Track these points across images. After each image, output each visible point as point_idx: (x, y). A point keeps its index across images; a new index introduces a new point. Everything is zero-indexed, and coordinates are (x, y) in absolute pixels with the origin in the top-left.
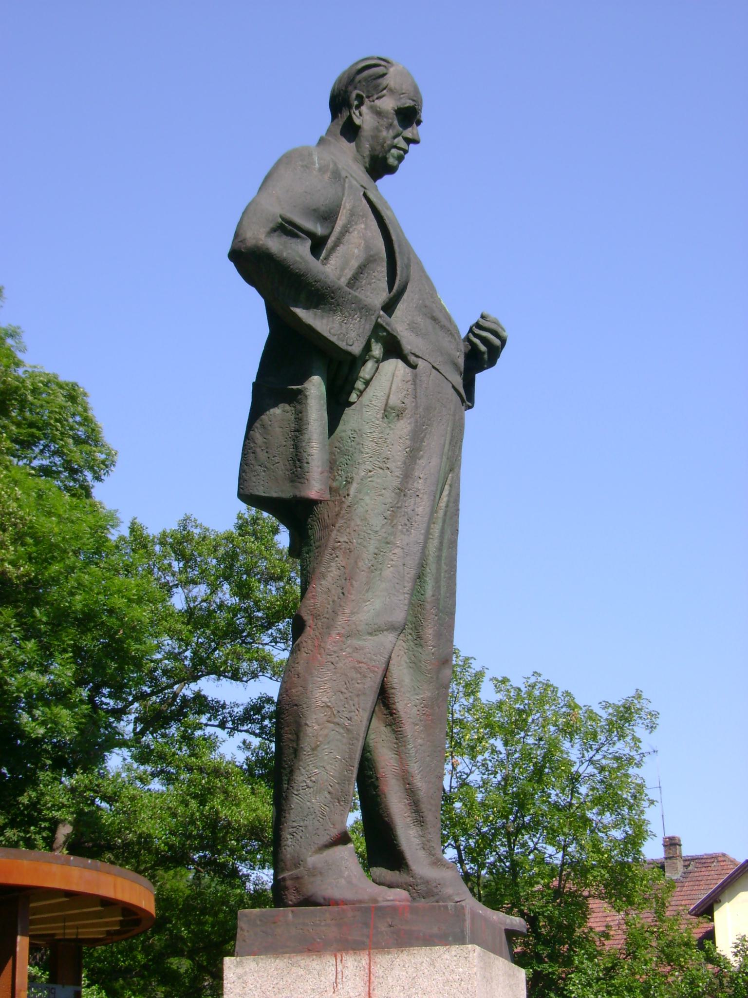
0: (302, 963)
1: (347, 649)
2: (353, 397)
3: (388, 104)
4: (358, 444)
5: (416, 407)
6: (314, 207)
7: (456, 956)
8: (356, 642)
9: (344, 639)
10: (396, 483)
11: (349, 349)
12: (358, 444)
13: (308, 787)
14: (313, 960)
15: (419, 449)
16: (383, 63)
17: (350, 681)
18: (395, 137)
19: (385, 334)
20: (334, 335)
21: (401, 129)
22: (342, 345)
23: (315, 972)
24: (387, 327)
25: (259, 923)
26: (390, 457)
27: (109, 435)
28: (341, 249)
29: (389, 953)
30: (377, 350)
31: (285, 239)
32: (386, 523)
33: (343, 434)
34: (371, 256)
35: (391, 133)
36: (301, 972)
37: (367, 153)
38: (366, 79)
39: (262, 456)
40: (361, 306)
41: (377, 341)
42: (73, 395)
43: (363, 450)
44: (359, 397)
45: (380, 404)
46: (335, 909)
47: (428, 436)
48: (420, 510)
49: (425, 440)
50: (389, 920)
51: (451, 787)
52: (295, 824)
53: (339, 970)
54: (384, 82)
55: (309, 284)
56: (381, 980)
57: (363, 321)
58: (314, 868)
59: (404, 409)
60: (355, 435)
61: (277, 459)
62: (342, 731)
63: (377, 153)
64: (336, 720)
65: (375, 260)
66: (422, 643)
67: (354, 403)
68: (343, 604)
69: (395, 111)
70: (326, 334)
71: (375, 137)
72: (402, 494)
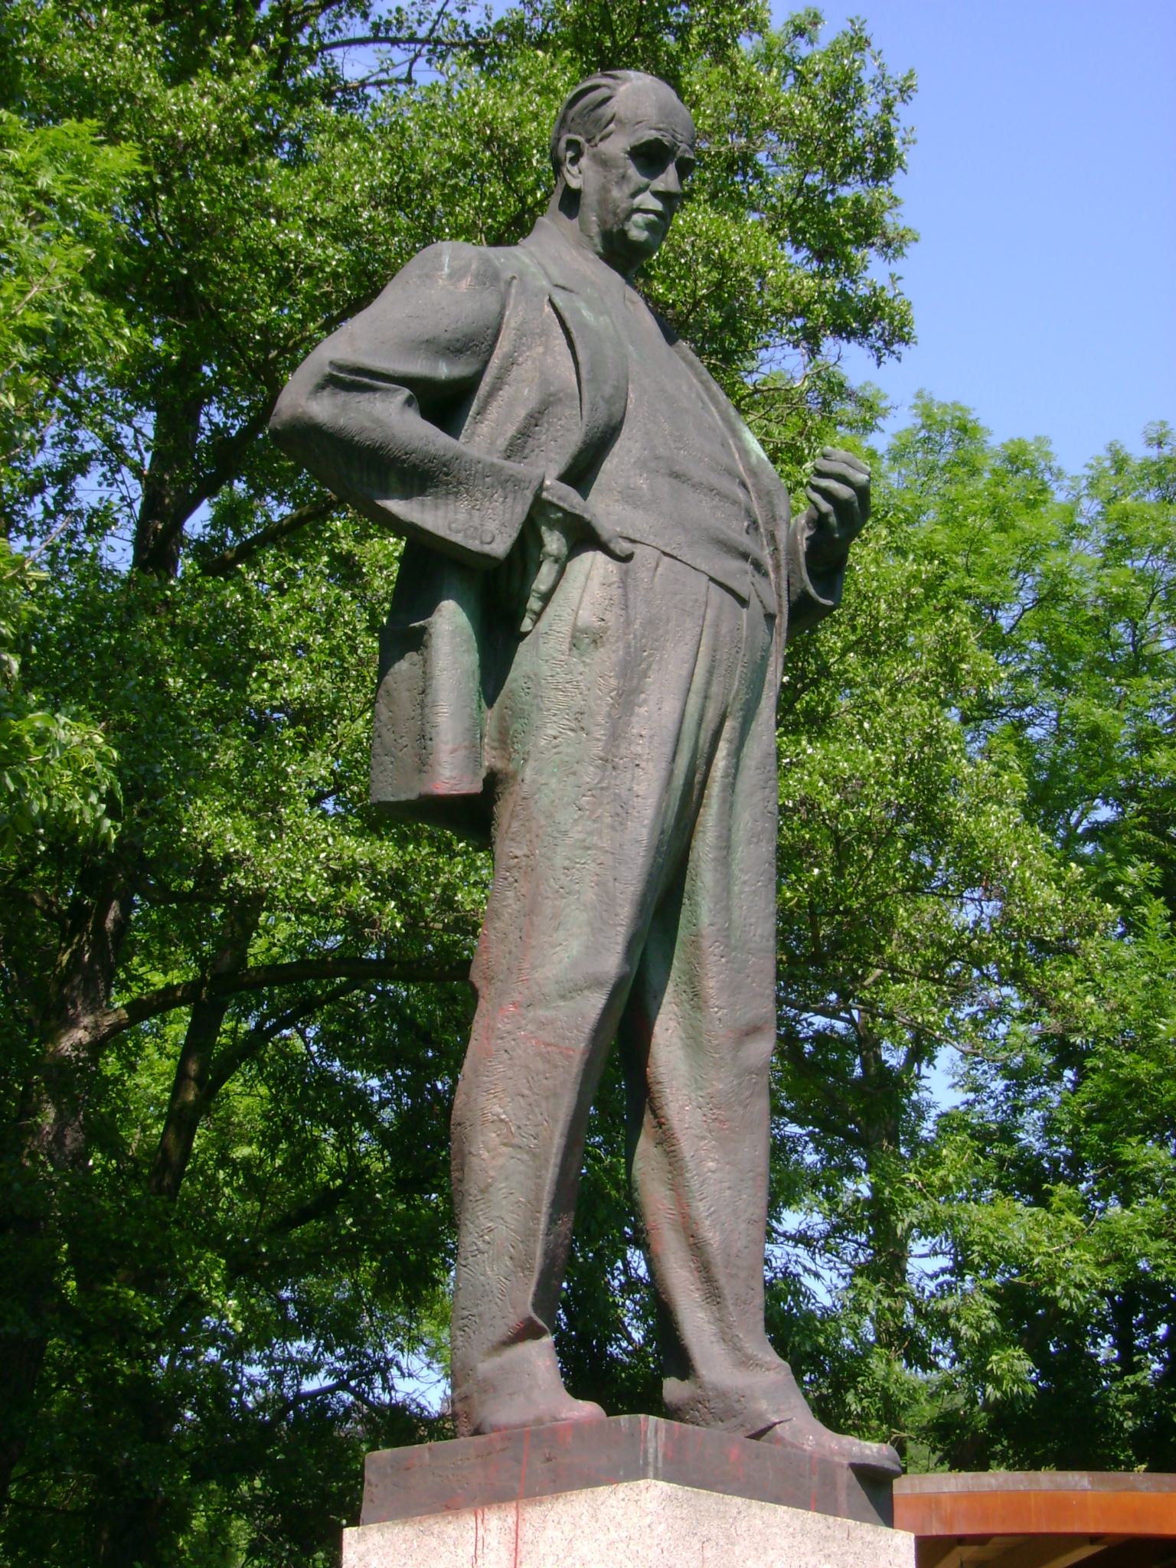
0: (436, 1529)
1: (529, 1027)
2: (526, 624)
3: (617, 145)
4: (536, 697)
5: (628, 623)
6: (426, 337)
8: (542, 1013)
9: (524, 1011)
10: (597, 750)
11: (487, 549)
12: (536, 697)
13: (482, 1252)
15: (638, 690)
18: (634, 195)
19: (560, 515)
20: (458, 532)
21: (646, 180)
22: (474, 545)
23: (450, 1542)
24: (561, 504)
25: (389, 1471)
26: (586, 710)
28: (505, 393)
30: (554, 542)
31: (343, 396)
32: (581, 817)
33: (514, 685)
34: (551, 395)
35: (627, 190)
36: (434, 1542)
37: (595, 230)
38: (581, 114)
39: (388, 737)
41: (551, 528)
44: (535, 622)
45: (566, 629)
47: (655, 667)
48: (640, 788)
49: (650, 673)
50: (547, 1451)
51: (934, 1253)
52: (466, 1313)
54: (607, 110)
55: (396, 460)
57: (509, 500)
59: (605, 630)
60: (530, 684)
61: (404, 741)
62: (525, 1157)
63: (608, 226)
64: (516, 1141)
65: (560, 400)
66: (701, 1004)
67: (527, 634)
69: (629, 153)
70: (442, 531)
71: (603, 202)
72: (609, 766)
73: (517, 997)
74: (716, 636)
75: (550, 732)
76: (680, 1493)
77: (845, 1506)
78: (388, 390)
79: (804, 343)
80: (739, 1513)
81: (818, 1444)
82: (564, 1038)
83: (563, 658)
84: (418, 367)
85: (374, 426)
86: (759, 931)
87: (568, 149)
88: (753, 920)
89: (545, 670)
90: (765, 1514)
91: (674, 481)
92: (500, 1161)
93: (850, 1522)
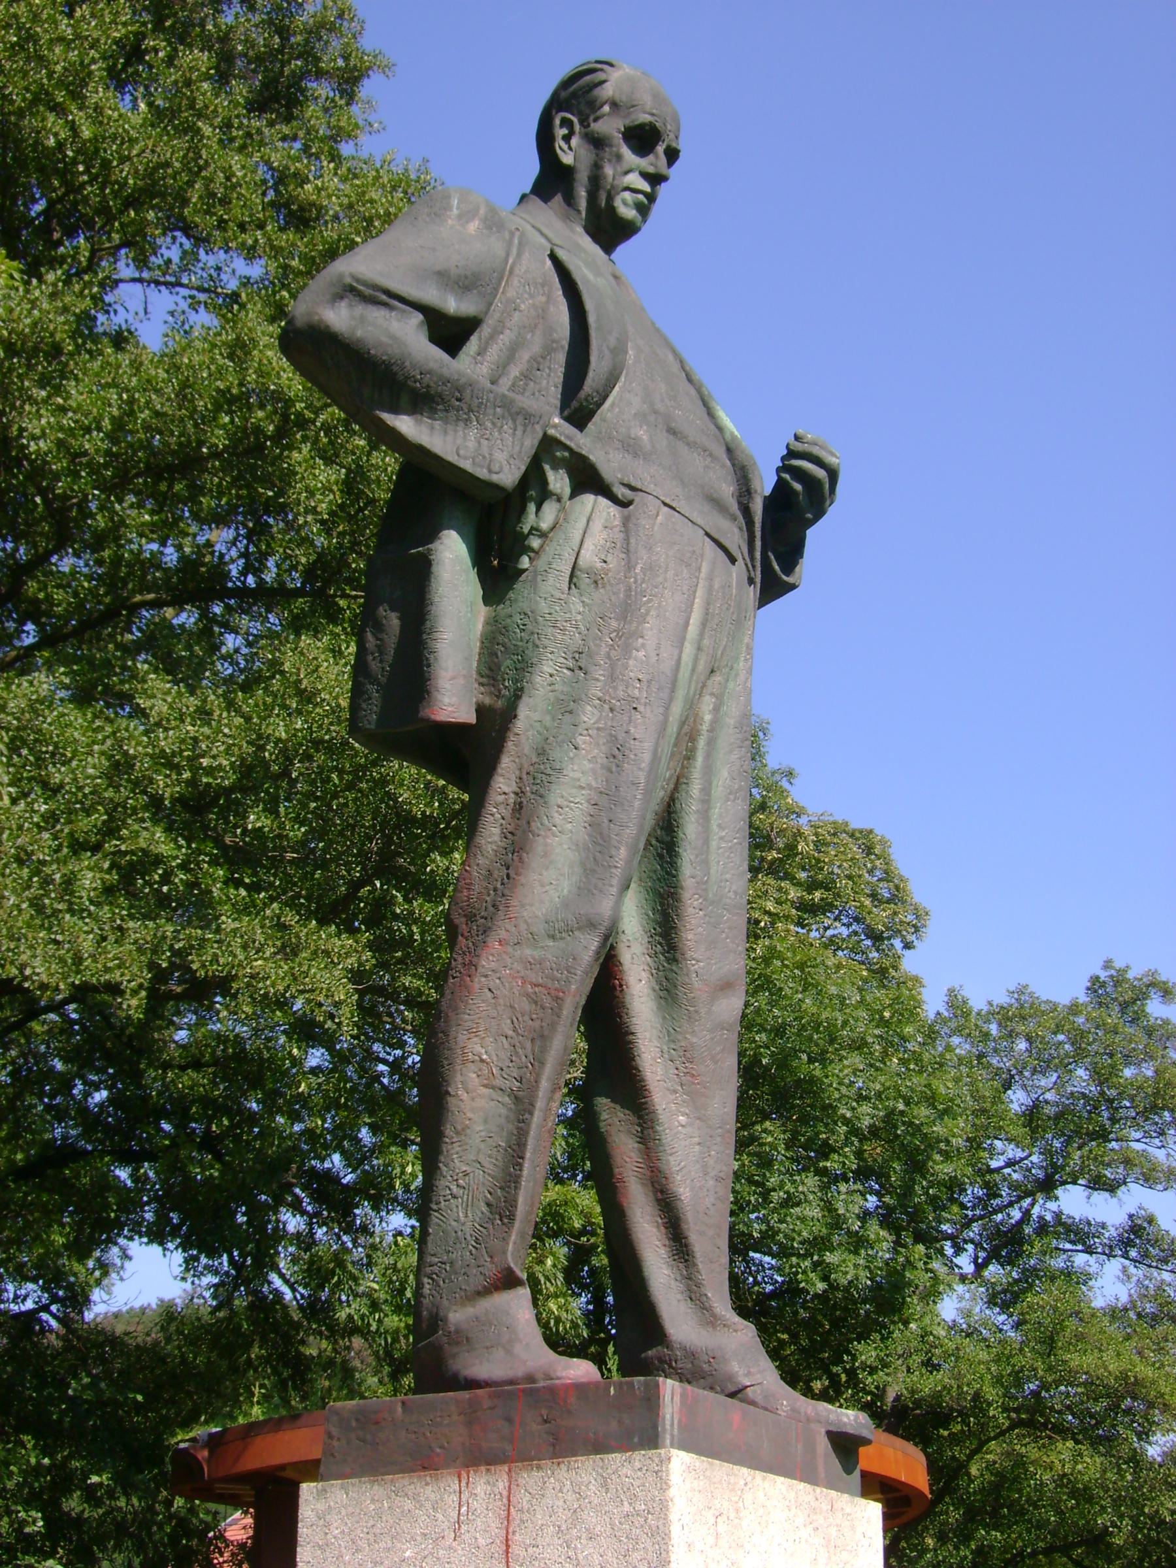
6: (438, 268)
7: (640, 1469)
9: (510, 949)
11: (495, 478)
13: (455, 1197)
14: (427, 1484)
16: (599, 66)
17: (519, 1016)
19: (566, 454)
20: (466, 458)
22: (482, 473)
23: (428, 1505)
24: (568, 443)
25: (354, 1424)
27: (919, 892)
29: (539, 1468)
30: (558, 481)
36: (408, 1504)
40: (513, 410)
41: (555, 468)
42: (868, 843)
43: (537, 642)
46: (465, 1395)
50: (544, 1412)
53: (464, 1499)
56: (525, 1516)
57: (519, 432)
58: (457, 1331)
60: (526, 621)
62: (507, 1100)
68: (506, 892)
70: (451, 458)
72: (606, 707)
73: (503, 934)
74: (710, 589)
75: (547, 669)
76: (697, 1464)
77: (823, 1475)
78: (404, 311)
79: (526, 530)
80: (746, 1484)
81: (793, 1410)
82: (553, 979)
83: (562, 597)
84: (431, 295)
85: (390, 342)
86: (734, 887)
87: (562, 126)
88: (728, 876)
89: (543, 607)
90: (766, 1484)
91: (671, 437)
92: (480, 1103)
93: (833, 1493)
